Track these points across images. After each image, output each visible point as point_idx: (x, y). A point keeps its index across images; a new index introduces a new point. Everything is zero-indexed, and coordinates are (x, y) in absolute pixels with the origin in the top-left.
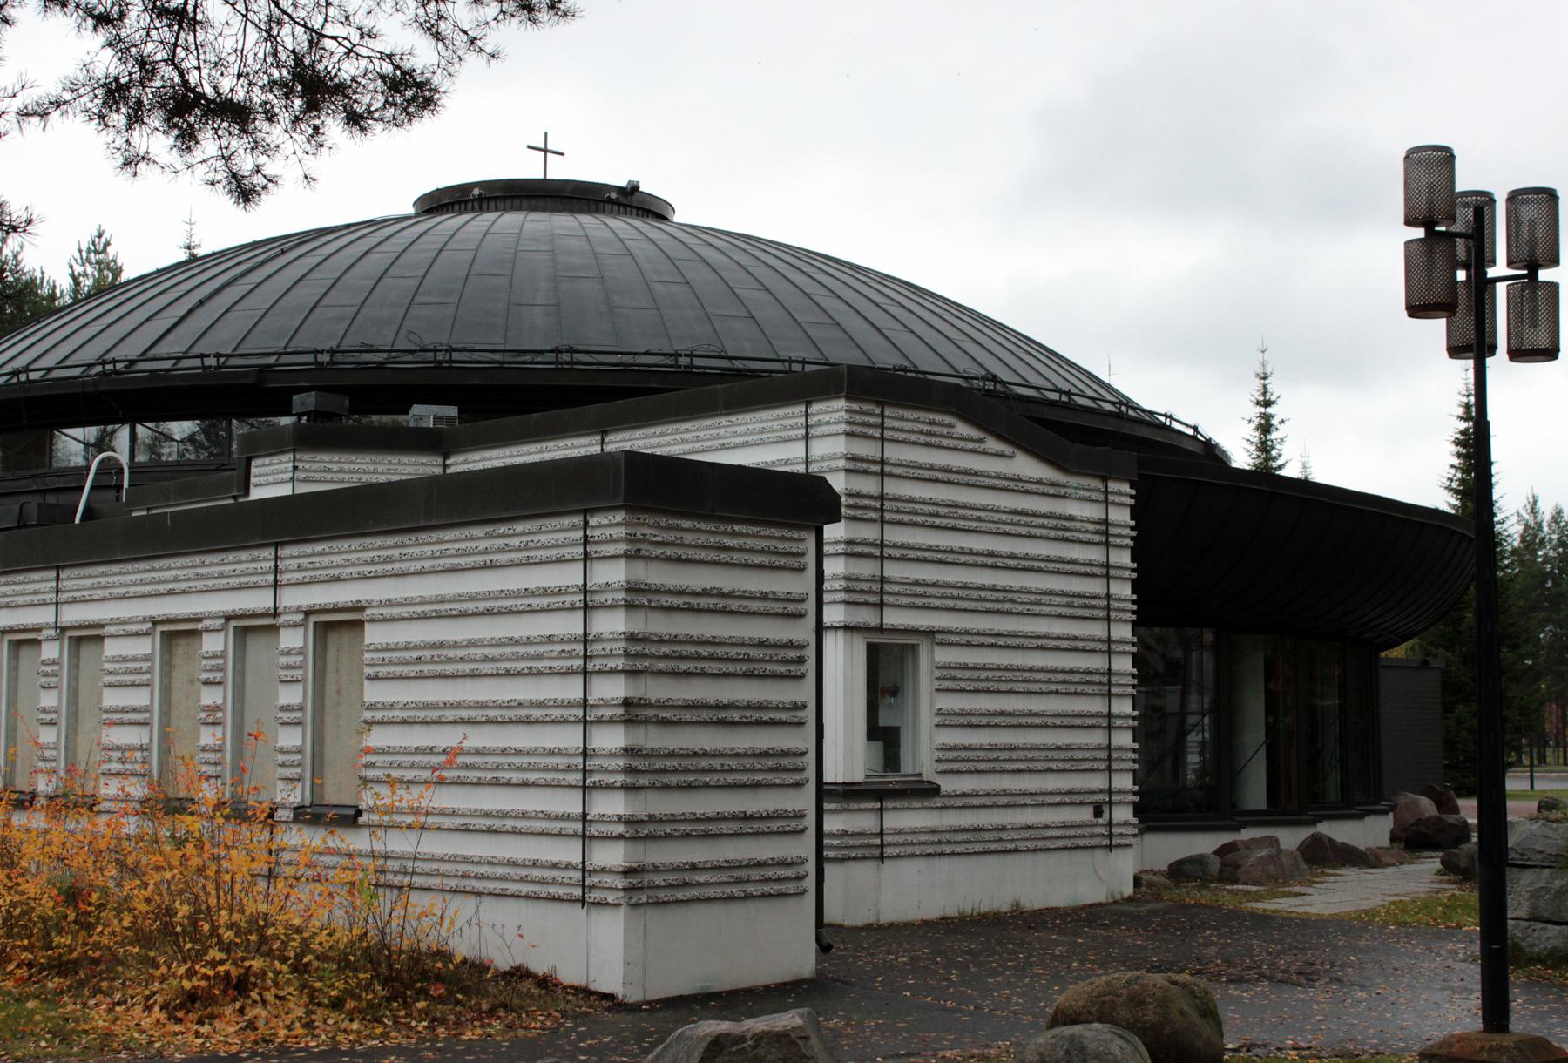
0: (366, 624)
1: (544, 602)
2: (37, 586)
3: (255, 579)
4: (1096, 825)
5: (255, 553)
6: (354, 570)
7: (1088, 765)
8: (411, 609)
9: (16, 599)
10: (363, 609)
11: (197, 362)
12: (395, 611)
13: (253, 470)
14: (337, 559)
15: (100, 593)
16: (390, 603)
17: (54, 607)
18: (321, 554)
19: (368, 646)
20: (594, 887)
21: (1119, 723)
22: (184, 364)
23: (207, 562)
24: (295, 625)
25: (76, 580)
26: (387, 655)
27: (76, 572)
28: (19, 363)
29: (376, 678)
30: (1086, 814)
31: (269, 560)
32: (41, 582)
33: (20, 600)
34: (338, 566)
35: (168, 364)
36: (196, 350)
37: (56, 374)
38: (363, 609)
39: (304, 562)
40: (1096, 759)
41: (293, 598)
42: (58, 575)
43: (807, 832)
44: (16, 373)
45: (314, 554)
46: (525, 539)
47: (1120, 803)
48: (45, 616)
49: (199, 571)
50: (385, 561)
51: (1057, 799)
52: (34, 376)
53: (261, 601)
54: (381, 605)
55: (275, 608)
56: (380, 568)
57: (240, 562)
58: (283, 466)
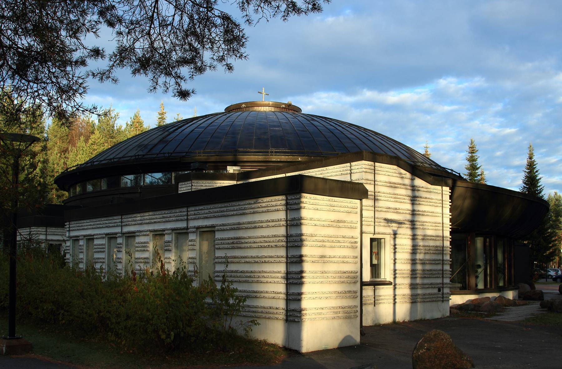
0: (216, 232)
1: (273, 224)
2: (115, 221)
3: (181, 218)
4: (439, 294)
5: (181, 210)
6: (212, 215)
7: (436, 276)
8: (230, 227)
9: (109, 225)
10: (215, 227)
11: (163, 155)
12: (225, 227)
13: (179, 186)
14: (207, 211)
15: (134, 223)
16: (223, 225)
17: (121, 227)
18: (201, 210)
19: (216, 238)
20: (290, 316)
21: (446, 262)
22: (159, 156)
23: (166, 213)
24: (193, 232)
25: (128, 219)
26: (223, 241)
27: (127, 216)
28: (112, 157)
29: (219, 249)
30: (436, 291)
31: (185, 212)
32: (117, 219)
33: (111, 225)
34: (207, 213)
35: (155, 156)
36: (162, 152)
37: (122, 159)
38: (215, 227)
39: (196, 212)
40: (439, 274)
41: (193, 224)
42: (122, 217)
43: (358, 298)
44: (111, 159)
45: (199, 210)
46: (267, 204)
47: (446, 287)
48: (118, 230)
49: (164, 215)
50: (222, 212)
51: (427, 286)
52: (115, 160)
53: (183, 225)
54: (220, 225)
55: (187, 227)
56: (220, 214)
57: (176, 213)
58: (188, 185)
